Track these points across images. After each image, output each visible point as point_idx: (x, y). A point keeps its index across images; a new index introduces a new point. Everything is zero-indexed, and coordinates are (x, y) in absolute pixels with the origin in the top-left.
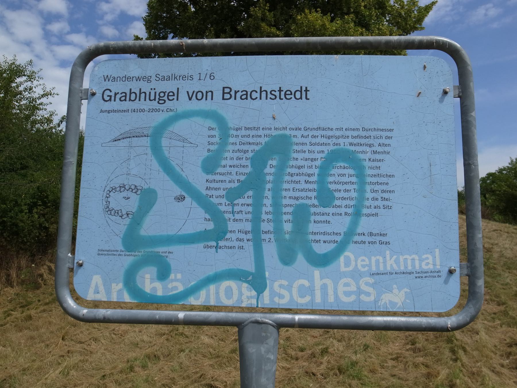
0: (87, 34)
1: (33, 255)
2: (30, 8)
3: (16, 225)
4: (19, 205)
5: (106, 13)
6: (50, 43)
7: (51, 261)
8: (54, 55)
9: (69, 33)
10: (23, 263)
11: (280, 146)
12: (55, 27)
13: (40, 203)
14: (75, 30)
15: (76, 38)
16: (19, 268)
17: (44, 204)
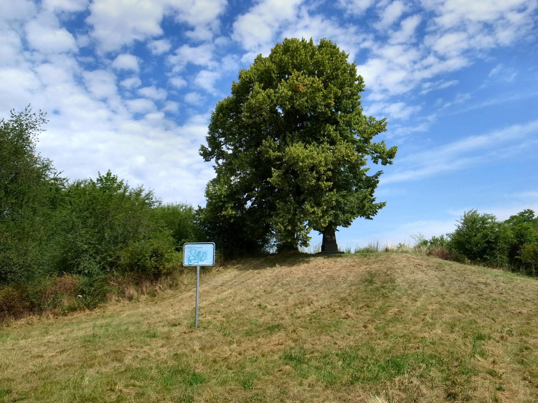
0: (158, 86)
1: (152, 281)
2: (105, 67)
3: (145, 267)
4: (145, 257)
5: (174, 65)
6: (124, 98)
7: (160, 284)
8: (128, 109)
9: (140, 87)
10: (148, 284)
11: (200, 252)
12: (128, 83)
13: (154, 255)
14: (146, 84)
15: (147, 91)
16: (146, 287)
17: (156, 255)
